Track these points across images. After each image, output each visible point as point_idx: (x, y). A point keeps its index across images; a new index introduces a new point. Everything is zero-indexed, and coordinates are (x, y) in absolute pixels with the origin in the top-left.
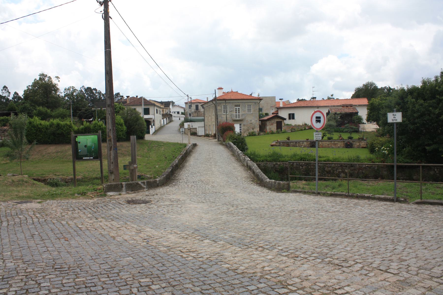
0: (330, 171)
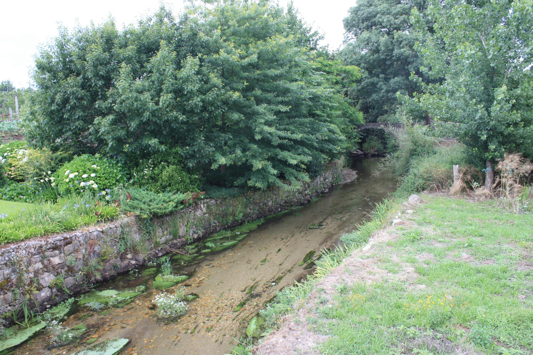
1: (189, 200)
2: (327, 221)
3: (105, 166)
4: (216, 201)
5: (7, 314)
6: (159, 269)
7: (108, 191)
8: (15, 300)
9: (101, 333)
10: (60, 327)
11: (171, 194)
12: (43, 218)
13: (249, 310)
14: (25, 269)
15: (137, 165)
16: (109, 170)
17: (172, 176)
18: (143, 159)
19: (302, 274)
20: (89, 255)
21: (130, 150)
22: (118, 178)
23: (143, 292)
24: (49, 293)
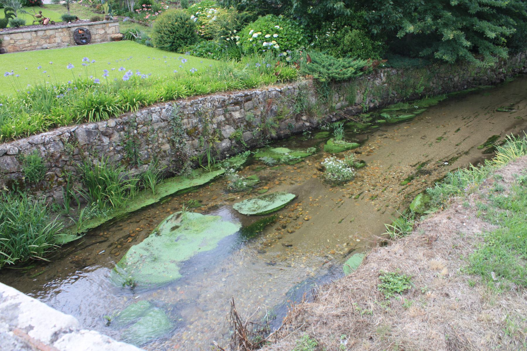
0: (195, 128)
1: (369, 67)
2: (519, 105)
3: (287, 27)
4: (398, 71)
5: (194, 158)
6: (331, 134)
7: (289, 52)
8: (201, 146)
9: (272, 186)
10: (236, 175)
11: (351, 59)
12: (227, 74)
13: (416, 186)
14: (210, 120)
15: (319, 27)
16: (292, 31)
17: (354, 41)
18: (326, 22)
19: (480, 158)
20: (267, 113)
21: (314, 12)
22: (300, 40)
23: (314, 153)
24: (229, 143)
